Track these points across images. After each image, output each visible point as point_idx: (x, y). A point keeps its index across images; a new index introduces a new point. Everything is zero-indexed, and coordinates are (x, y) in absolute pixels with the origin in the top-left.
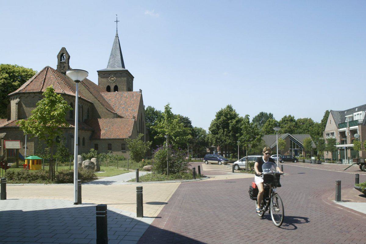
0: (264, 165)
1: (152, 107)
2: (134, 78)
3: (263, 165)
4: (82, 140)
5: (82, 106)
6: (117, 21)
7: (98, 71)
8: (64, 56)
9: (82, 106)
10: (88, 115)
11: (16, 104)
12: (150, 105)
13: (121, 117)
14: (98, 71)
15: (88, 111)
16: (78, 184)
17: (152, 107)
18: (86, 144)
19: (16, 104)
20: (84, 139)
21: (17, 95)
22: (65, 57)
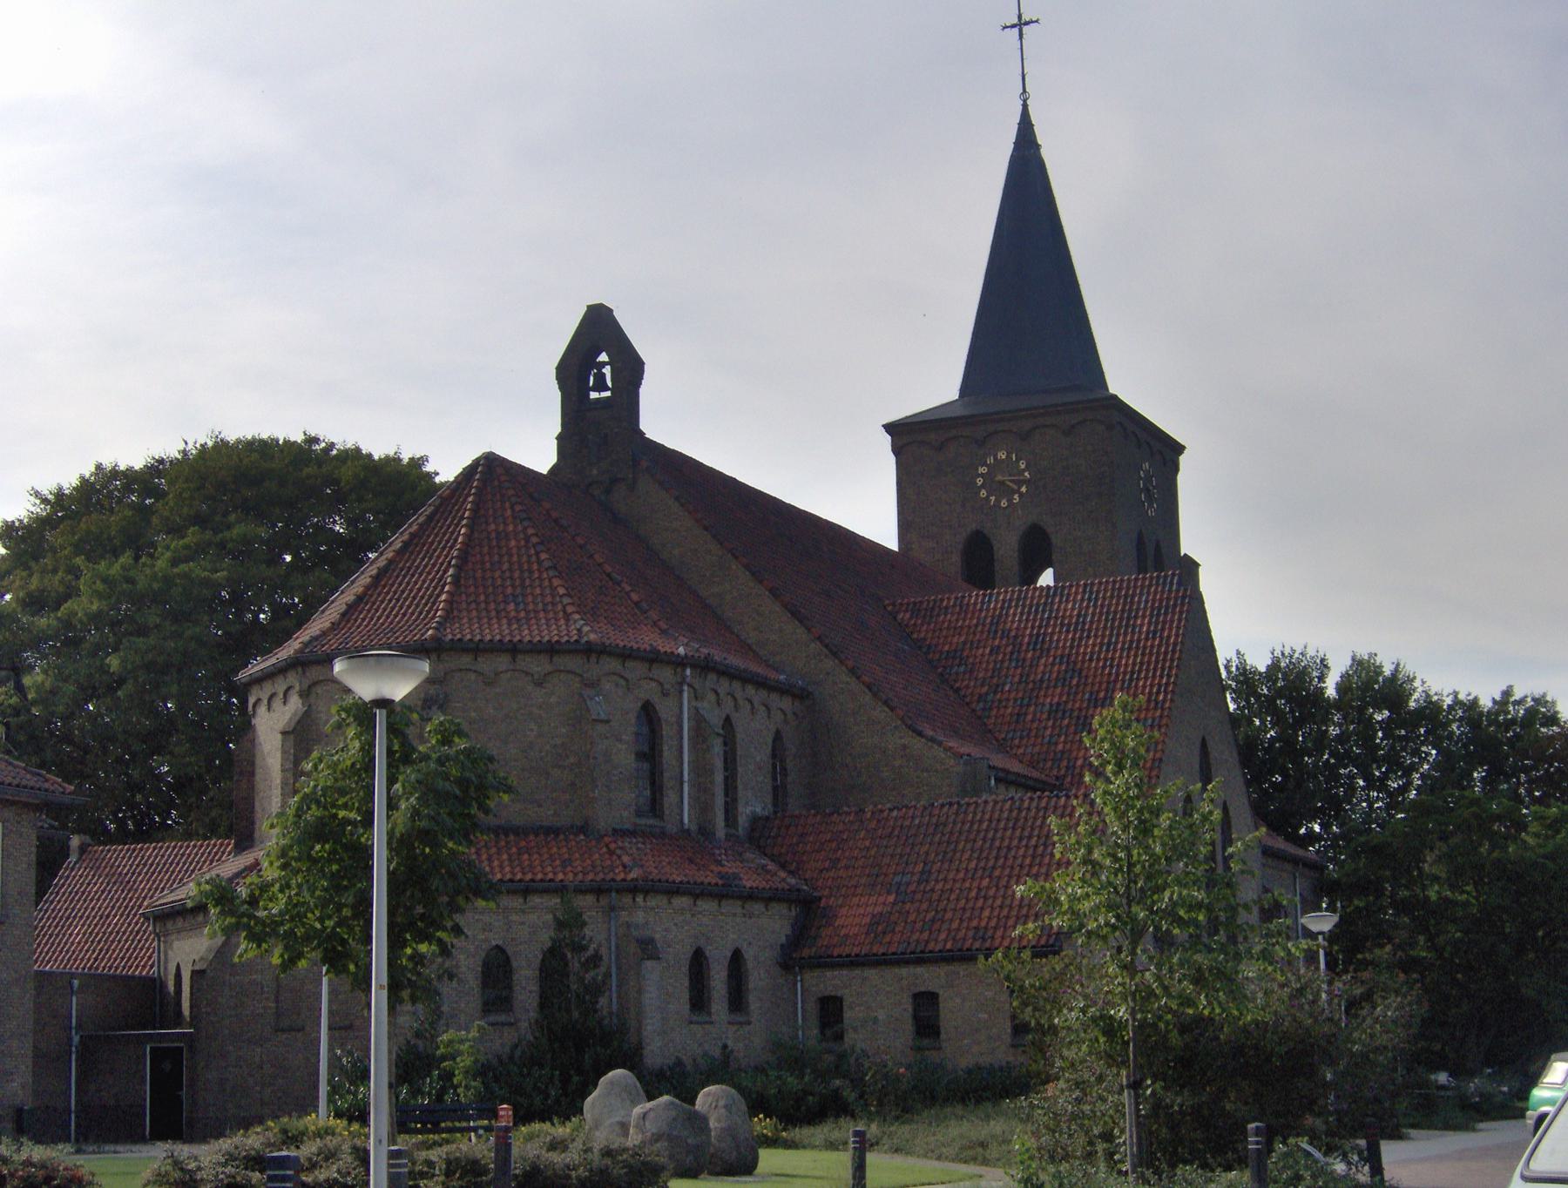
0: (709, 1094)
1: (1387, 670)
2: (1178, 449)
3: (711, 1088)
4: (724, 974)
5: (728, 719)
6: (1021, 24)
7: (889, 428)
8: (604, 364)
9: (728, 719)
10: (775, 789)
11: (284, 733)
12: (1363, 653)
13: (1204, 739)
14: (889, 428)
15: (777, 752)
16: (391, 1166)
17: (1387, 670)
18: (754, 1003)
19: (284, 733)
20: (737, 958)
21: (293, 678)
22: (607, 371)
